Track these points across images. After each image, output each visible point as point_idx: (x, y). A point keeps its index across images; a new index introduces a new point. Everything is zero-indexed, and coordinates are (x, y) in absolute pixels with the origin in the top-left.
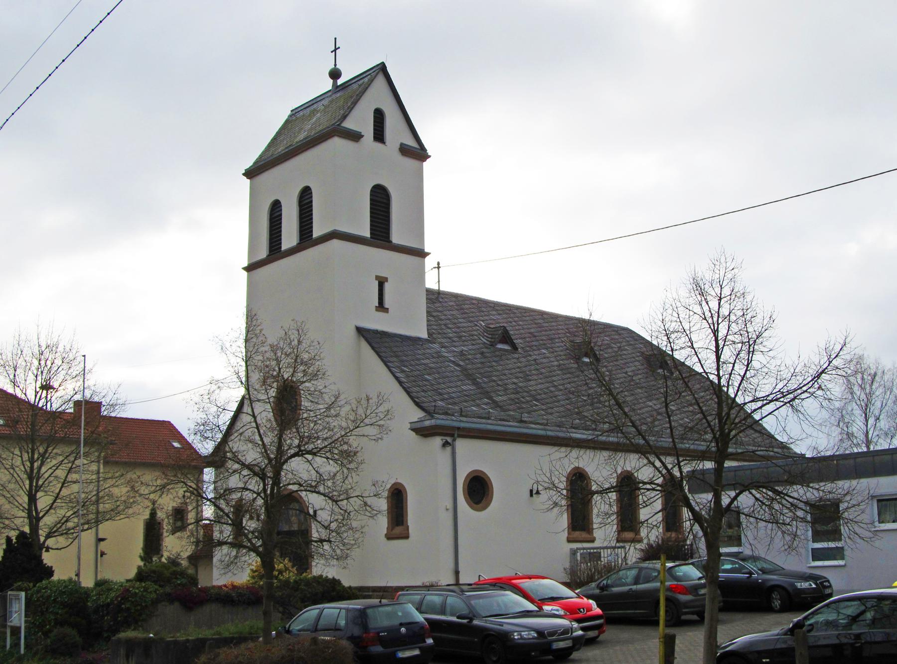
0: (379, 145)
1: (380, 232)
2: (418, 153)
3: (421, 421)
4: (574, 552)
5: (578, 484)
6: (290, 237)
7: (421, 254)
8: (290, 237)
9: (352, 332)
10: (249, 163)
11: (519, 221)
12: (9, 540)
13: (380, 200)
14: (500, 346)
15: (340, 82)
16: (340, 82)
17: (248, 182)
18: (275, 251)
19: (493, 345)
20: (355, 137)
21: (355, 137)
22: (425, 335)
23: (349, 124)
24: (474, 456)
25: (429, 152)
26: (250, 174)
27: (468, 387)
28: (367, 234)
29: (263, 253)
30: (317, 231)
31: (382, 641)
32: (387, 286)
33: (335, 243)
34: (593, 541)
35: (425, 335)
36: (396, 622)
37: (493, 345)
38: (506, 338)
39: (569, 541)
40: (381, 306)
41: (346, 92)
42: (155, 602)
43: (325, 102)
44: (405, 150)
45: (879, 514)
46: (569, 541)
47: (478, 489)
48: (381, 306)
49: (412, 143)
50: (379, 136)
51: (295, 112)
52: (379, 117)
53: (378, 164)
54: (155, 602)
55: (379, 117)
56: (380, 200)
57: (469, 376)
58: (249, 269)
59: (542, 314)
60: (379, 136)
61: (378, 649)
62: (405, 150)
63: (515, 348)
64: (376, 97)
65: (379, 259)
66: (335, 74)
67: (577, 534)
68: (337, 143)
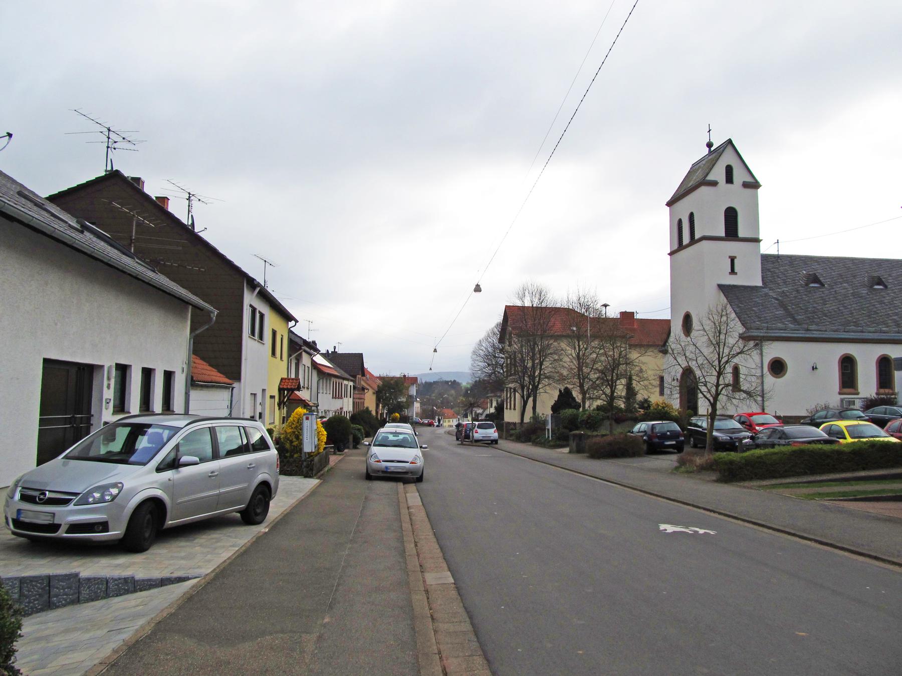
0: (729, 185)
1: (731, 232)
2: (753, 185)
3: (744, 333)
4: (842, 400)
5: (848, 365)
6: (686, 240)
7: (757, 240)
8: (686, 240)
9: (716, 287)
10: (669, 198)
11: (797, 222)
12: (560, 391)
13: (731, 216)
14: (812, 285)
15: (712, 149)
16: (712, 149)
17: (668, 208)
18: (681, 247)
19: (807, 285)
20: (714, 184)
21: (714, 184)
22: (760, 284)
23: (710, 177)
24: (773, 350)
25: (761, 183)
26: (670, 204)
27: (780, 312)
28: (723, 234)
29: (676, 247)
30: (697, 236)
31: (658, 437)
32: (736, 261)
33: (704, 242)
34: (858, 394)
35: (760, 284)
36: (666, 429)
37: (807, 285)
38: (816, 279)
39: (840, 394)
40: (733, 271)
41: (714, 153)
42: (603, 420)
43: (704, 162)
44: (746, 185)
45: (301, 424)
46: (840, 394)
47: (778, 367)
48: (733, 271)
49: (749, 179)
50: (729, 179)
51: (694, 165)
52: (729, 170)
53: (732, 195)
54: (603, 420)
55: (729, 170)
56: (731, 216)
57: (782, 305)
58: (671, 254)
59: (853, 261)
60: (729, 179)
61: (657, 440)
62: (746, 185)
63: (822, 285)
64: (727, 158)
65: (732, 247)
66: (709, 145)
67: (846, 390)
68: (703, 189)
